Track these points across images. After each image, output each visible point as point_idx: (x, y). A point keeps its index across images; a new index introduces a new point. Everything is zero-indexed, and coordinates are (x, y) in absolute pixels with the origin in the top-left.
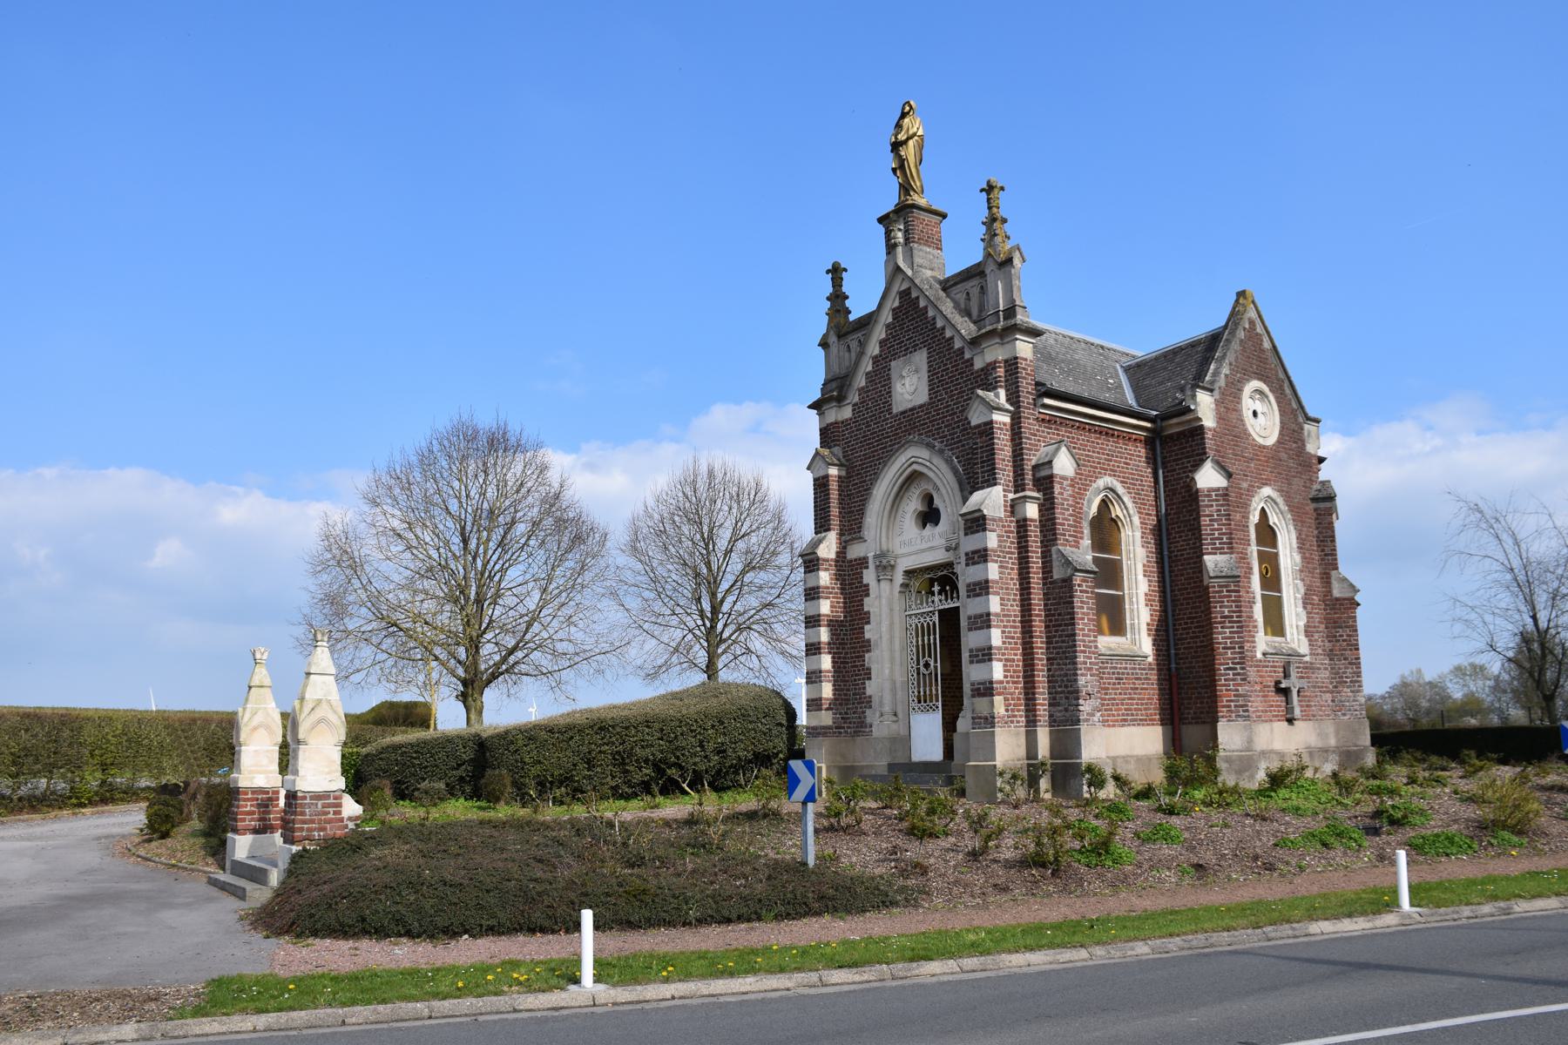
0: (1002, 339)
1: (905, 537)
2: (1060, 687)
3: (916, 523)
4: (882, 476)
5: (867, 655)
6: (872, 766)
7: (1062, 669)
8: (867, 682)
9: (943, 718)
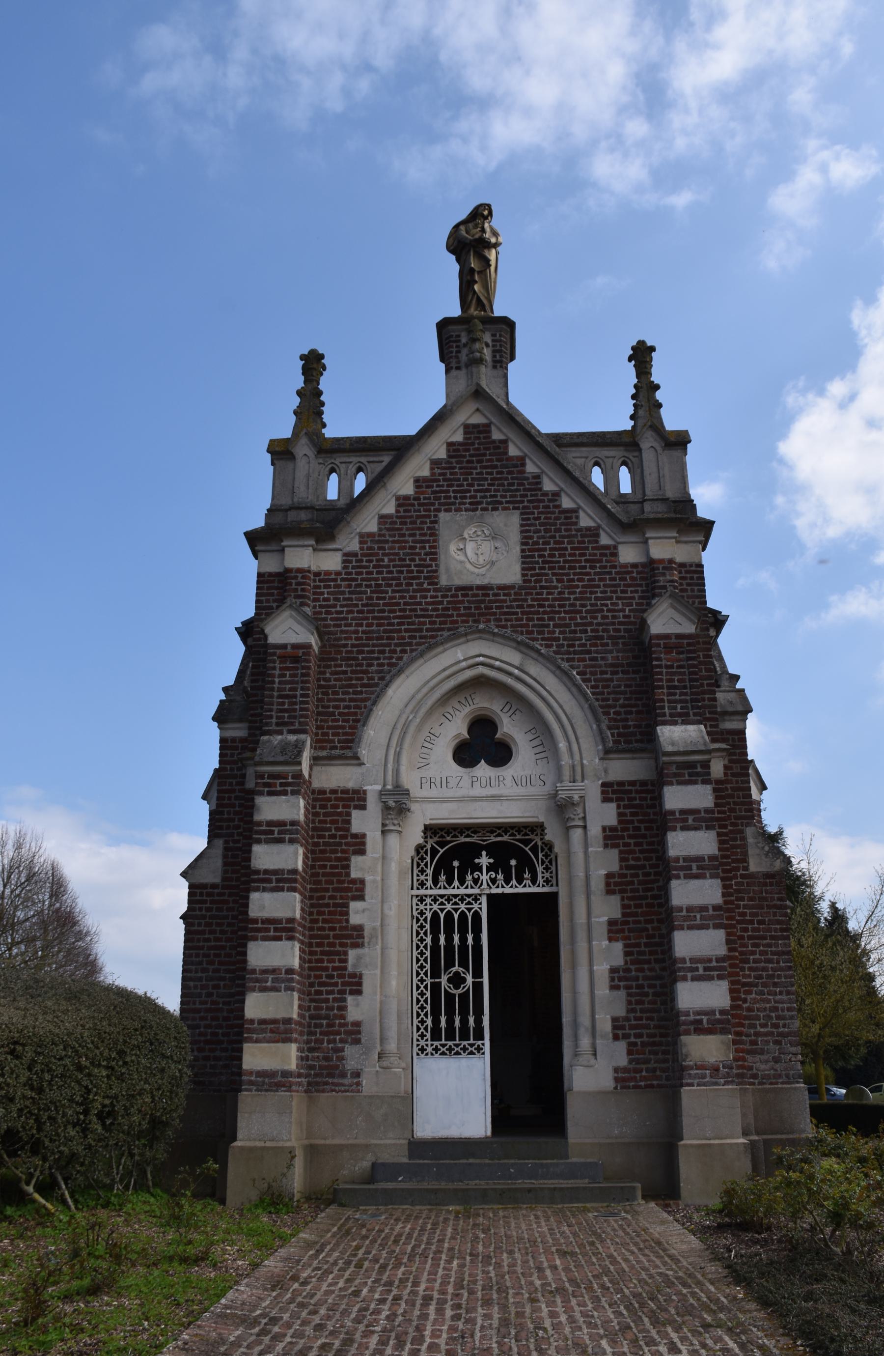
0: (317, 542)
1: (431, 772)
2: (762, 1026)
5: (352, 954)
6: (367, 1146)
7: (769, 1001)
8: (350, 999)
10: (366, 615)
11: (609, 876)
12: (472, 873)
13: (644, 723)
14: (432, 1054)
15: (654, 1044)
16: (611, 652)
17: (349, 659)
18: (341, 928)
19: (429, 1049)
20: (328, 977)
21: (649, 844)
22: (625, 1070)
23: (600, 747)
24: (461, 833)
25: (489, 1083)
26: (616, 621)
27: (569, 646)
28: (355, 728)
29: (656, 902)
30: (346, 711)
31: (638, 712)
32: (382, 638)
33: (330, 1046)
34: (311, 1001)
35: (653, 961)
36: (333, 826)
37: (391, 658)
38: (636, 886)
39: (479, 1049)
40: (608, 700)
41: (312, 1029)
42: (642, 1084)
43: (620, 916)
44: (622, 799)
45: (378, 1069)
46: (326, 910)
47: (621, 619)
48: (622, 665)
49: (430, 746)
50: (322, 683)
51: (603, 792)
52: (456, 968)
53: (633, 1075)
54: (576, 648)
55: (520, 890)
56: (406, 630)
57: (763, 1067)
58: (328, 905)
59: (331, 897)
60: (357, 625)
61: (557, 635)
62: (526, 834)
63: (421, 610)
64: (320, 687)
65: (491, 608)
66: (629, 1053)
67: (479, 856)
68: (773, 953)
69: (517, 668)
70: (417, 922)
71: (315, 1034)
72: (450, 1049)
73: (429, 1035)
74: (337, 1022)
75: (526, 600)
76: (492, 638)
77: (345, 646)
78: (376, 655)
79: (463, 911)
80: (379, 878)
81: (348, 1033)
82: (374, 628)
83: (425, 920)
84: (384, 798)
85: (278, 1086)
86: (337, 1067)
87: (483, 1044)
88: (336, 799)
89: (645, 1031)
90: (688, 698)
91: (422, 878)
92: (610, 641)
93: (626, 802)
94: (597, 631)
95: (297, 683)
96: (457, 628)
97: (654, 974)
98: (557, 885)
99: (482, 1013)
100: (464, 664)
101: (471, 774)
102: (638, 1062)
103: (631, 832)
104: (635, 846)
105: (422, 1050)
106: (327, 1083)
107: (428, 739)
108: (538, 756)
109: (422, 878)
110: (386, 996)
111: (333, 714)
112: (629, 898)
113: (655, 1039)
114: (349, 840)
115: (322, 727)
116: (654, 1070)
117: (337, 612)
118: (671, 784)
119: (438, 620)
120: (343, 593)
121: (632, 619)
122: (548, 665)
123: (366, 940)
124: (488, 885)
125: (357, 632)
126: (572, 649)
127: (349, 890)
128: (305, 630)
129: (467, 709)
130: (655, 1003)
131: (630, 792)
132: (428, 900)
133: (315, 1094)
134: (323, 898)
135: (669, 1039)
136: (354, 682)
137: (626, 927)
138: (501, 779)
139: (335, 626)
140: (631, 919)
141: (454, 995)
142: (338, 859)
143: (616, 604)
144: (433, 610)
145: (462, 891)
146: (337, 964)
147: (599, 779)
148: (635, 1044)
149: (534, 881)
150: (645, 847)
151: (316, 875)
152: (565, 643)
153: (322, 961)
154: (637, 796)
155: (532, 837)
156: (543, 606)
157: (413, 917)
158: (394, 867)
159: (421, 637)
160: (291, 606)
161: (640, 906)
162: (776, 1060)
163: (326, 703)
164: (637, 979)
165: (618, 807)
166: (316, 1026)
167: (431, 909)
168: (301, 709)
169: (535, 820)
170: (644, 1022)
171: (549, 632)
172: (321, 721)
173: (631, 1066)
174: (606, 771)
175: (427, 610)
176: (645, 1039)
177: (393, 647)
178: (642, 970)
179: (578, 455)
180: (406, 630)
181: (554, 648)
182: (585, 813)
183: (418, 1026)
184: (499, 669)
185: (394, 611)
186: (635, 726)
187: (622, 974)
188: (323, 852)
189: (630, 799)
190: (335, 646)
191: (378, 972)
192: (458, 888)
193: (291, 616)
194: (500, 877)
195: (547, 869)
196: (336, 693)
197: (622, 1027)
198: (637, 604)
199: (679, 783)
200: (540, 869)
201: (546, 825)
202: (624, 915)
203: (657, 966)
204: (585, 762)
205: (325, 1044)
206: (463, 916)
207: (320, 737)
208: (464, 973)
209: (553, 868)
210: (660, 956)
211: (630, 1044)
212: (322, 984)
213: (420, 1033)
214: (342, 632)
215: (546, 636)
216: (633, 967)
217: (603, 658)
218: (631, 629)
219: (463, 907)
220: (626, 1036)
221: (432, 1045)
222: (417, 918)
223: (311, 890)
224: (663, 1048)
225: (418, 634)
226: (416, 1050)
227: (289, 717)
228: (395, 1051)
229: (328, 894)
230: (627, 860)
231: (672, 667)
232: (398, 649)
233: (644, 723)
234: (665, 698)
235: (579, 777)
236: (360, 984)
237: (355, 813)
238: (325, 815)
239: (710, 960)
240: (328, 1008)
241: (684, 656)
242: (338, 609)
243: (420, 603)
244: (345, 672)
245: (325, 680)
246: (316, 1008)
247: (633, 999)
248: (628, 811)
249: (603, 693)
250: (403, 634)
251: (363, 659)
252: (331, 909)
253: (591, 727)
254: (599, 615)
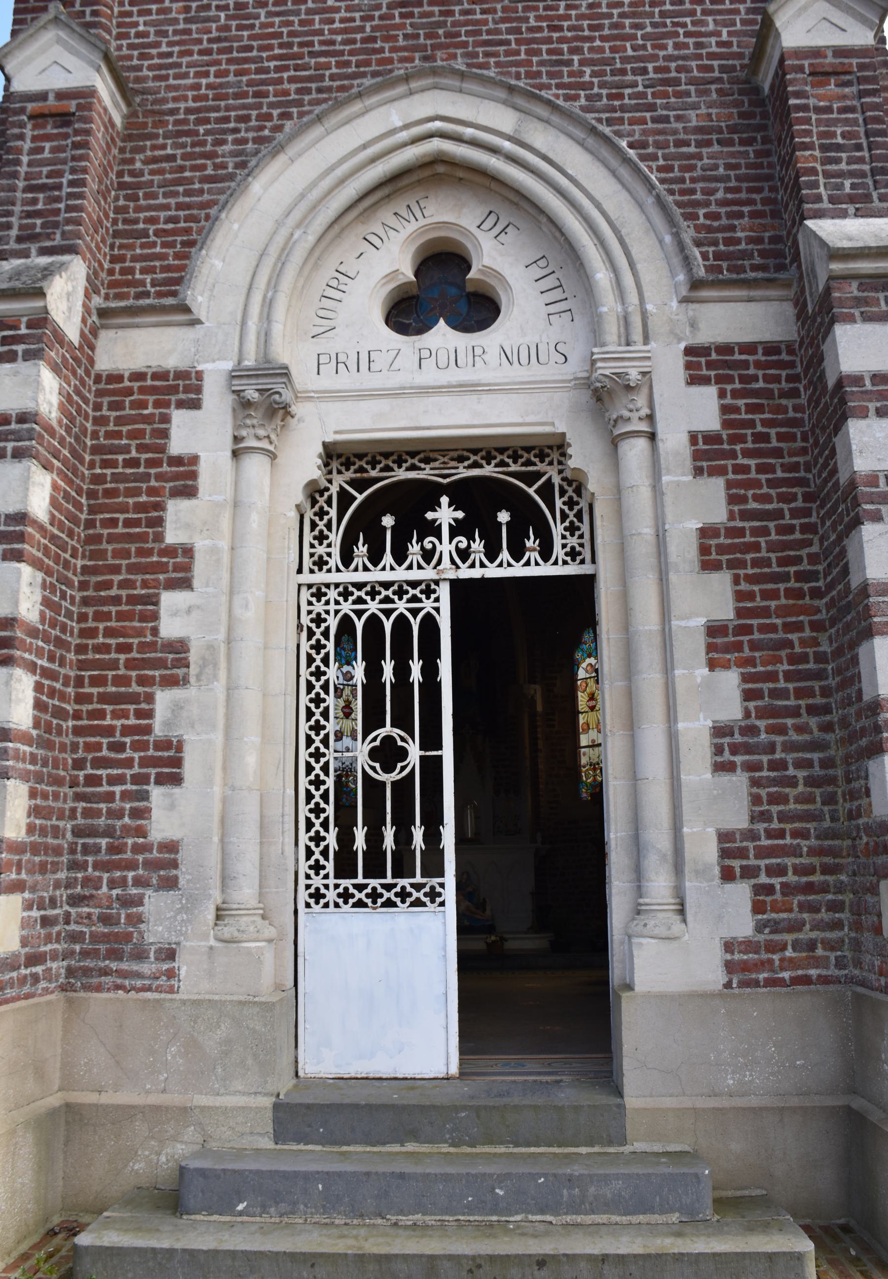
3: (383, 302)
4: (292, 150)
6: (185, 1110)
8: (157, 793)
9: (462, 930)
10: (215, 56)
11: (706, 532)
12: (420, 540)
13: (767, 234)
14: (337, 905)
15: (809, 888)
16: (695, 106)
17: (179, 134)
18: (143, 647)
19: (331, 895)
20: (112, 747)
21: (786, 468)
22: (748, 945)
23: (681, 277)
24: (400, 462)
25: (455, 966)
26: (704, 51)
27: (610, 97)
28: (186, 256)
29: (806, 587)
30: (170, 226)
31: (753, 215)
32: (245, 95)
33: (115, 892)
34: (78, 797)
35: (803, 711)
36: (134, 443)
37: (261, 128)
38: (764, 554)
39: (433, 895)
40: (693, 192)
41: (79, 857)
42: (786, 975)
43: (731, 615)
44: (729, 379)
45: (212, 942)
46: (113, 609)
47: (714, 49)
48: (720, 131)
49: (336, 295)
50: (127, 179)
51: (688, 366)
52: (388, 730)
53: (764, 956)
54: (626, 101)
55: (518, 571)
56: (291, 80)
58: (116, 600)
59: (123, 585)
60: (198, 75)
61: (587, 78)
62: (529, 463)
63: (321, 43)
64: (122, 186)
65: (459, 35)
66: (758, 908)
67: (434, 505)
69: (510, 138)
70: (309, 638)
71: (83, 866)
72: (374, 895)
73: (330, 867)
74: (130, 841)
75: (527, 20)
76: (457, 84)
77: (173, 112)
78: (232, 125)
79: (402, 615)
80: (224, 544)
81: (152, 865)
82: (231, 78)
83: (326, 634)
84: (237, 384)
86: (128, 937)
87: (442, 885)
88: (142, 390)
89: (789, 861)
90: (866, 167)
91: (321, 550)
92: (692, 88)
93: (737, 386)
94: (667, 70)
95: (64, 162)
96: (391, 71)
97: (807, 737)
98: (593, 561)
99: (440, 821)
100: (404, 135)
101: (418, 345)
102: (776, 927)
103: (750, 445)
104: (758, 471)
105: (317, 896)
106: (106, 972)
107: (334, 283)
108: (552, 309)
109: (321, 550)
110: (233, 788)
111: (145, 234)
112: (750, 579)
113: (811, 878)
114: (165, 468)
115: (121, 259)
116: (811, 946)
117: (161, 55)
118: (851, 319)
119: (353, 59)
120: (175, 21)
121: (735, 49)
122: (571, 128)
123: (193, 670)
124: (453, 561)
125: (197, 87)
126: (617, 103)
127: (161, 568)
128: (84, 65)
129: (412, 226)
130: (810, 799)
131: (745, 364)
132: (332, 594)
133: (82, 994)
134: (108, 585)
135: (843, 877)
136: (187, 174)
137: (745, 638)
138: (478, 351)
139: (156, 78)
140: (755, 622)
141: (383, 784)
142: (141, 508)
143: (703, 23)
144: (345, 42)
145: (401, 574)
146: (132, 721)
147: (680, 340)
148: (769, 889)
149: (546, 553)
150: (780, 474)
151: (96, 539)
152: (604, 92)
153: (101, 715)
154: (760, 373)
155: (540, 467)
156: (560, 29)
157: (300, 627)
158: (255, 522)
159: (319, 90)
160: (56, 20)
161: (773, 595)
163: (132, 215)
164: (771, 748)
165: (722, 394)
166: (86, 850)
167: (337, 612)
168: (69, 209)
169: (547, 429)
170: (788, 840)
171: (571, 74)
172: (121, 247)
173: (761, 938)
174: (693, 324)
175: (332, 43)
176: (791, 878)
177: (265, 110)
178: (781, 730)
180: (291, 80)
181: (583, 101)
182: (651, 406)
183: (308, 848)
184: (474, 143)
185: (270, 48)
186: (750, 240)
187: (738, 738)
188: (108, 493)
189: (743, 379)
190: (153, 112)
191: (218, 737)
192: (392, 568)
193: (59, 40)
194: (478, 546)
195: (572, 529)
196: (154, 196)
197: (742, 854)
198: (744, 22)
199: (868, 318)
200: (557, 530)
201: (569, 438)
202: (740, 613)
203: (813, 722)
204: (649, 307)
205: (105, 889)
206: (402, 624)
207: (117, 276)
208: (403, 739)
209: (585, 528)
210: (819, 700)
211: (759, 890)
212: (100, 763)
213: (312, 862)
214: (169, 88)
215: (566, 80)
216: (762, 724)
217: (678, 118)
218: (734, 66)
219: (401, 606)
220: (749, 873)
221: (337, 886)
222: (309, 629)
223: (85, 570)
224: (830, 897)
225: (314, 86)
226: (303, 895)
227: (43, 226)
228: (253, 903)
229: (117, 578)
230: (743, 500)
231: (828, 110)
232: (275, 113)
233: (767, 234)
234: (819, 168)
235: (637, 335)
236: (177, 762)
237: (179, 417)
238: (119, 421)
240: (111, 814)
241: (854, 89)
242: (164, 49)
243: (320, 32)
244: (171, 158)
245: (132, 173)
246: (87, 813)
247: (763, 792)
248: (741, 402)
249: (682, 180)
250: (286, 86)
251: (208, 133)
252: (124, 608)
253: (661, 241)
254: (670, 43)
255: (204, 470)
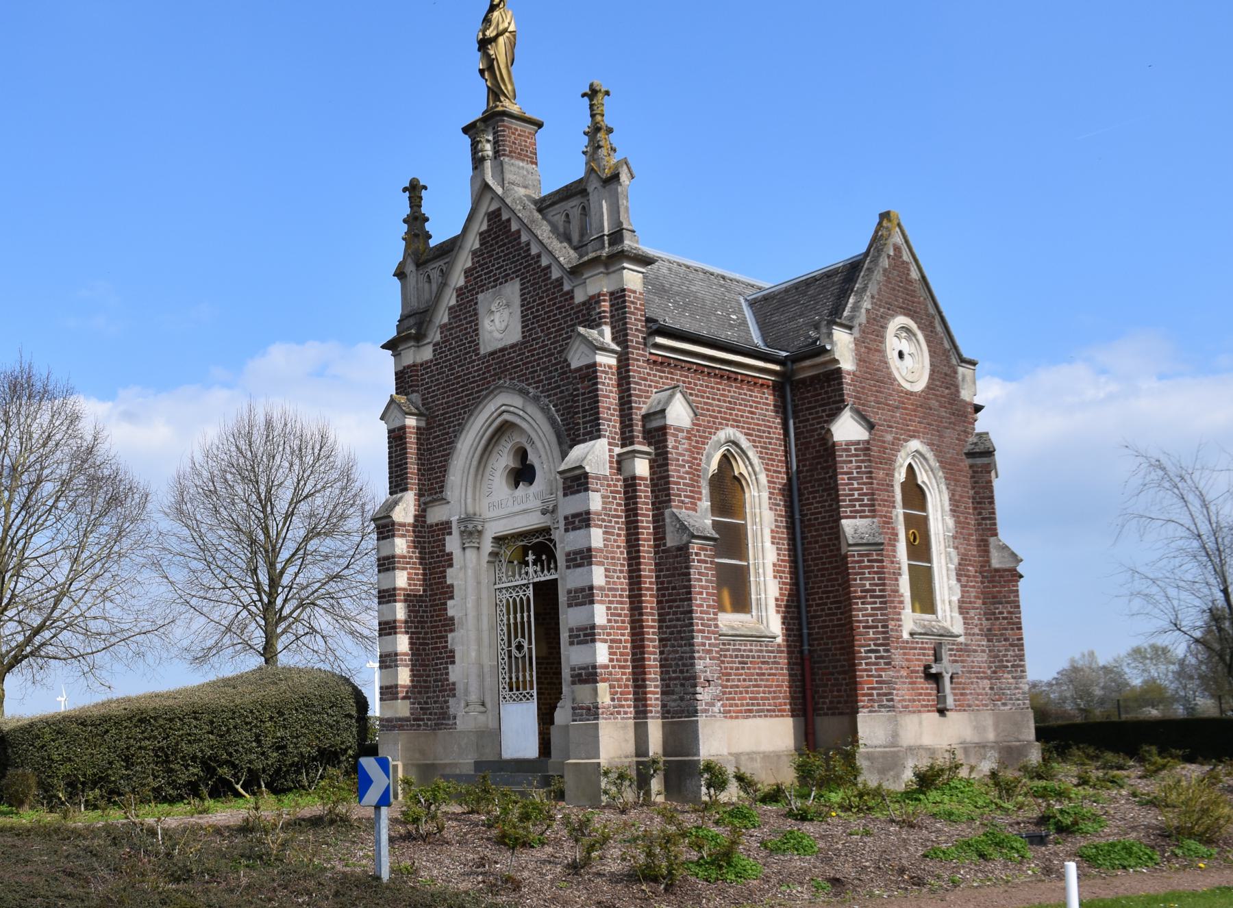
3: (507, 482)
4: (467, 428)
5: (450, 635)
6: (456, 764)
9: (539, 709)
57: (673, 704)
68: (682, 613)
85: (394, 727)
106: (442, 724)
162: (682, 699)
179: (554, 213)
239: (586, 629)
255: (454, 556)
